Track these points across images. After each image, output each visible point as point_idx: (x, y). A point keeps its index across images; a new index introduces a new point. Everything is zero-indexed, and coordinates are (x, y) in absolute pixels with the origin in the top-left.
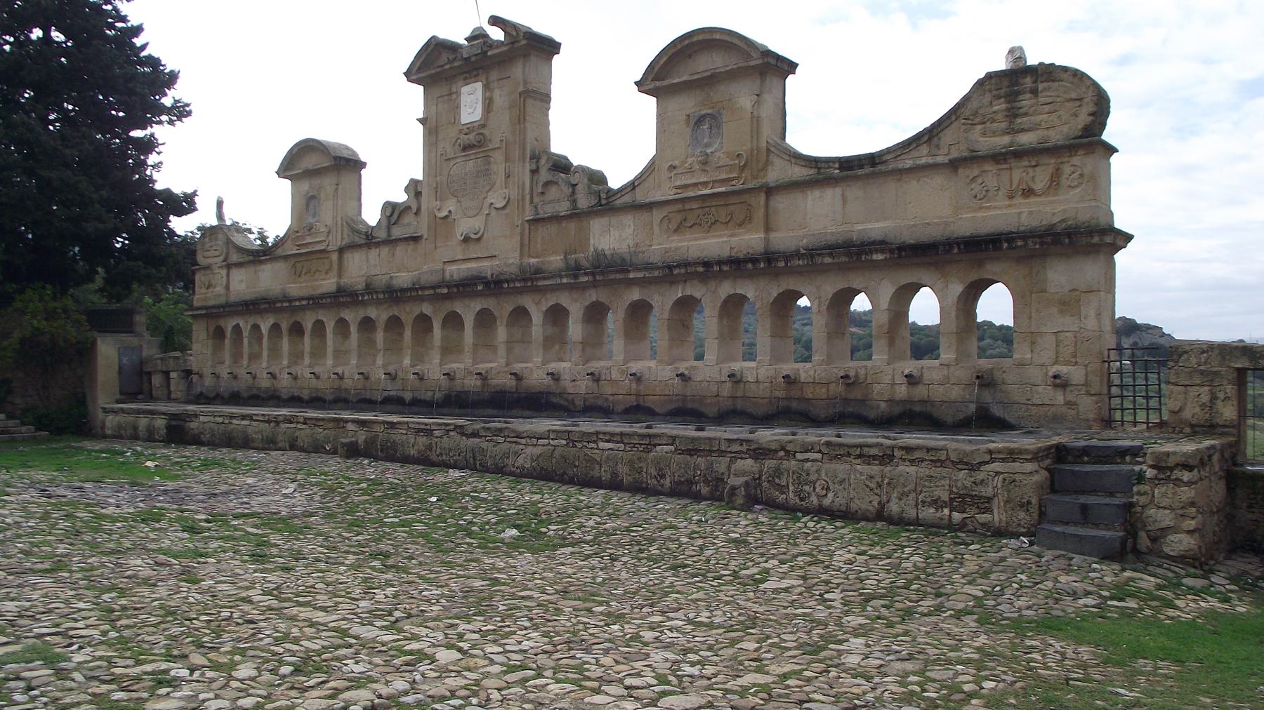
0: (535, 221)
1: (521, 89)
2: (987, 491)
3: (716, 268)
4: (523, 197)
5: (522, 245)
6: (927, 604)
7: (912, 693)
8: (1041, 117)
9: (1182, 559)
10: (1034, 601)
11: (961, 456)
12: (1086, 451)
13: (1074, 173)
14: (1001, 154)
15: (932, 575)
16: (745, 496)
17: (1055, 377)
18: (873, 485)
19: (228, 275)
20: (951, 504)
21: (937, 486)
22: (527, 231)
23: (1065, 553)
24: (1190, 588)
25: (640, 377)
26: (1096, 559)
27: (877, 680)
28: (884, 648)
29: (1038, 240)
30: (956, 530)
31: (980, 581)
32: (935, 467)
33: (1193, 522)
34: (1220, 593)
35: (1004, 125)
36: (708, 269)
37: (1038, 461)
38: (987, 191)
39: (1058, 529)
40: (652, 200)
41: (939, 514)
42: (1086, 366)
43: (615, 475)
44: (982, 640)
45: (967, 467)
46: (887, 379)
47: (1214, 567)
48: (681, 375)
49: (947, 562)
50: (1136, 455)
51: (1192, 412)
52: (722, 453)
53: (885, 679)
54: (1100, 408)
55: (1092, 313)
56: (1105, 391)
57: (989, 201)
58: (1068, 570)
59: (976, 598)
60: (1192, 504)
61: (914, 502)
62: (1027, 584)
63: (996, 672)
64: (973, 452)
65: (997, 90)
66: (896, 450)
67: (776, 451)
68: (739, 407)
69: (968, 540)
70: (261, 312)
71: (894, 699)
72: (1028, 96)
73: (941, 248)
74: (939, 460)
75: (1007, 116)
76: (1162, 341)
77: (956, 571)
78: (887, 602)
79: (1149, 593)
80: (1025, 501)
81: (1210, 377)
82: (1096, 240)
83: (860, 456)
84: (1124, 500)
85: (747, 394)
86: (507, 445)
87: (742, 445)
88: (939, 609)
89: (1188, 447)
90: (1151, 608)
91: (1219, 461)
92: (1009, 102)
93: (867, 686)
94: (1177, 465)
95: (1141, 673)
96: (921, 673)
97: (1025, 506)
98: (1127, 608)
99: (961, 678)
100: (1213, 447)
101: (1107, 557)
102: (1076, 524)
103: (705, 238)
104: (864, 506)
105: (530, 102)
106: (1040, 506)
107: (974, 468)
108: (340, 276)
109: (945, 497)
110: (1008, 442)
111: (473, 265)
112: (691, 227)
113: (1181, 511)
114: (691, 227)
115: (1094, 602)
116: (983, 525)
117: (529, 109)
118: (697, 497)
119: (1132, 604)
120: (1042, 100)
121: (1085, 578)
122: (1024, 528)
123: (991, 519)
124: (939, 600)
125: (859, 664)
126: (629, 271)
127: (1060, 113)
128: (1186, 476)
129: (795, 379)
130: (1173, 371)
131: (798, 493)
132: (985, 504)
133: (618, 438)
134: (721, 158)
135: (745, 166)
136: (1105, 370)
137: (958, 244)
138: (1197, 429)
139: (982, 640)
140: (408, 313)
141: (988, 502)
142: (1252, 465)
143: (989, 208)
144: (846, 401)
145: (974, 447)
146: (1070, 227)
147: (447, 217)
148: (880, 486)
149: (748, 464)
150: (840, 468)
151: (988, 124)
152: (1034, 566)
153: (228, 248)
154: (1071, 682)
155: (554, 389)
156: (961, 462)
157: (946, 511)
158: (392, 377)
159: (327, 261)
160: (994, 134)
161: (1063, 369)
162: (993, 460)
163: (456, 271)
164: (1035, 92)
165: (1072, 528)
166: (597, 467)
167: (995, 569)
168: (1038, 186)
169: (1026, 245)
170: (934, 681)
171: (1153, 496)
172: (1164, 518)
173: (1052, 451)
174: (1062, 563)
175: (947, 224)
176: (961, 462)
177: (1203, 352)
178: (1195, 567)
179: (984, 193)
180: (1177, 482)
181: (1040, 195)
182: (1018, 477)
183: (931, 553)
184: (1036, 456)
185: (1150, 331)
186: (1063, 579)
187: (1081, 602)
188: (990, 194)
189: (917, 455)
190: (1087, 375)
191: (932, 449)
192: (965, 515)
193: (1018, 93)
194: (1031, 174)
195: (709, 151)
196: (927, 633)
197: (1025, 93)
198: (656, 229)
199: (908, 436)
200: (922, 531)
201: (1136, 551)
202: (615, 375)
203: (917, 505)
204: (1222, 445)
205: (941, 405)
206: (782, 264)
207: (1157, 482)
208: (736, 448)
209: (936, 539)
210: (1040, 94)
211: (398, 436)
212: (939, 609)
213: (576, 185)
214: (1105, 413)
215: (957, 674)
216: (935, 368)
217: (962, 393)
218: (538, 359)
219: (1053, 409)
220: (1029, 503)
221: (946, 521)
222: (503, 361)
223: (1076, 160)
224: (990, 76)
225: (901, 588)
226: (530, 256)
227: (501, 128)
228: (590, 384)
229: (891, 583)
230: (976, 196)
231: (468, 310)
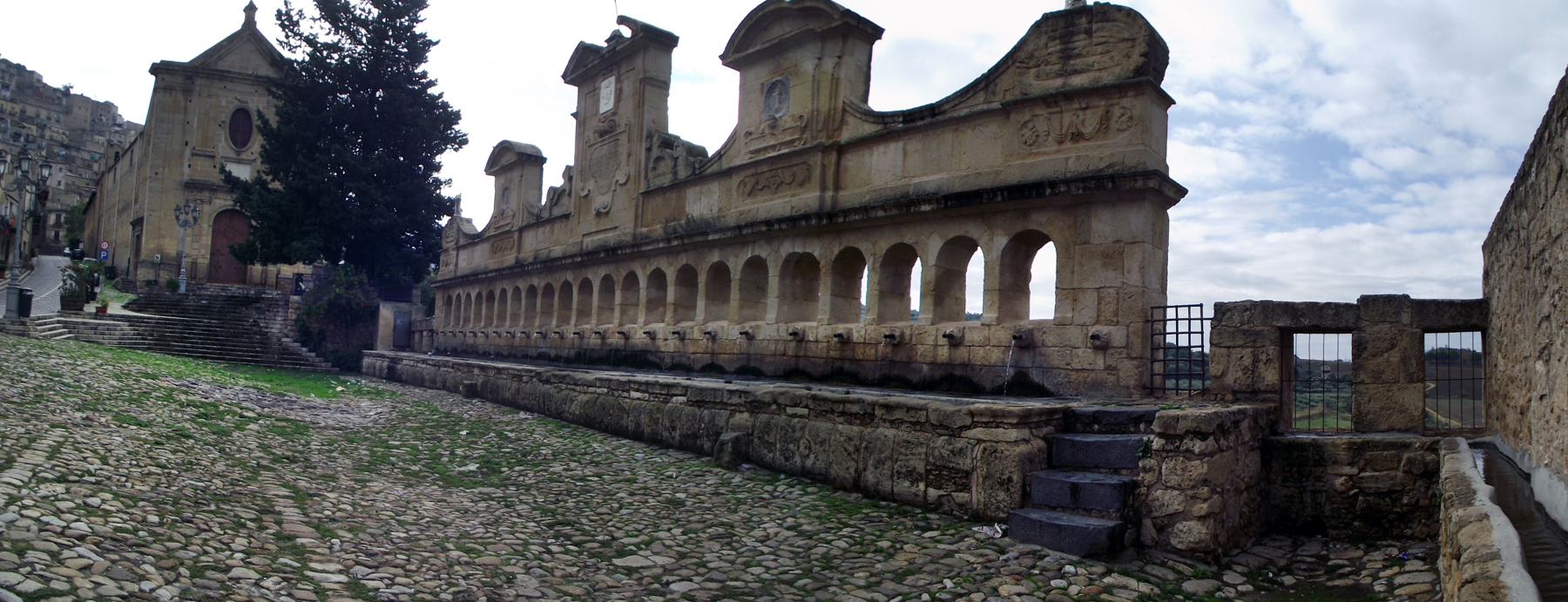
0: (648, 194)
1: (641, 76)
2: (965, 463)
3: (776, 227)
4: (639, 173)
5: (636, 217)
8: (1093, 58)
12: (1096, 417)
13: (1123, 115)
14: (1052, 95)
16: (732, 453)
17: (1093, 337)
18: (851, 449)
19: (457, 255)
21: (913, 454)
22: (641, 204)
25: (715, 336)
26: (1075, 558)
29: (1081, 185)
32: (915, 431)
33: (1205, 506)
35: (1057, 67)
36: (771, 229)
37: (1030, 428)
38: (1037, 136)
40: (732, 165)
41: (913, 489)
42: (1128, 326)
43: (638, 425)
45: (947, 432)
46: (930, 340)
48: (746, 333)
52: (724, 405)
54: (1141, 373)
55: (1135, 267)
57: (1039, 147)
64: (953, 413)
65: (1053, 31)
66: (876, 407)
67: (769, 404)
68: (801, 366)
70: (471, 283)
72: (1083, 36)
73: (986, 196)
74: (918, 423)
75: (1061, 58)
80: (1005, 477)
82: (1139, 184)
83: (843, 414)
85: (809, 354)
86: (567, 392)
87: (740, 397)
91: (1251, 429)
92: (1064, 43)
94: (1187, 432)
97: (1006, 484)
102: (1064, 509)
103: (772, 200)
104: (842, 473)
105: (648, 88)
106: (1024, 486)
107: (955, 433)
108: (519, 251)
109: (921, 468)
111: (601, 236)
112: (762, 190)
113: (1190, 490)
114: (762, 190)
116: (961, 505)
117: (647, 95)
118: (699, 452)
120: (1095, 40)
122: (1004, 512)
123: (969, 499)
126: (708, 235)
127: (1113, 54)
128: (1198, 446)
129: (849, 338)
131: (784, 451)
132: (962, 480)
133: (643, 388)
134: (787, 122)
135: (806, 126)
138: (1239, 396)
140: (557, 280)
143: (1037, 154)
144: (893, 363)
145: (958, 408)
147: (587, 196)
148: (857, 450)
149: (743, 418)
150: (823, 425)
151: (1042, 67)
153: (458, 234)
155: (650, 348)
156: (941, 426)
157: (922, 486)
158: (544, 336)
159: (511, 240)
160: (1048, 76)
161: (1103, 329)
162: (974, 425)
163: (590, 242)
164: (1089, 33)
166: (626, 416)
168: (1088, 130)
169: (1068, 191)
171: (1160, 473)
173: (1056, 417)
175: (997, 173)
176: (941, 426)
177: (1247, 310)
178: (1208, 564)
179: (1034, 138)
180: (1188, 455)
181: (1089, 140)
182: (1001, 447)
188: (1040, 140)
189: (898, 415)
190: (1128, 336)
192: (942, 492)
193: (1073, 34)
194: (1081, 117)
195: (777, 116)
197: (1079, 33)
198: (734, 193)
202: (697, 335)
203: (892, 476)
206: (841, 220)
207: (1164, 455)
208: (735, 400)
210: (1094, 35)
211: (504, 381)
213: (677, 158)
214: (1146, 379)
216: (977, 328)
217: (1002, 356)
218: (641, 320)
219: (1093, 375)
221: (920, 499)
222: (616, 321)
223: (1126, 102)
224: (1047, 17)
226: (642, 226)
227: (626, 115)
228: (677, 342)
230: (1026, 142)
231: (596, 276)
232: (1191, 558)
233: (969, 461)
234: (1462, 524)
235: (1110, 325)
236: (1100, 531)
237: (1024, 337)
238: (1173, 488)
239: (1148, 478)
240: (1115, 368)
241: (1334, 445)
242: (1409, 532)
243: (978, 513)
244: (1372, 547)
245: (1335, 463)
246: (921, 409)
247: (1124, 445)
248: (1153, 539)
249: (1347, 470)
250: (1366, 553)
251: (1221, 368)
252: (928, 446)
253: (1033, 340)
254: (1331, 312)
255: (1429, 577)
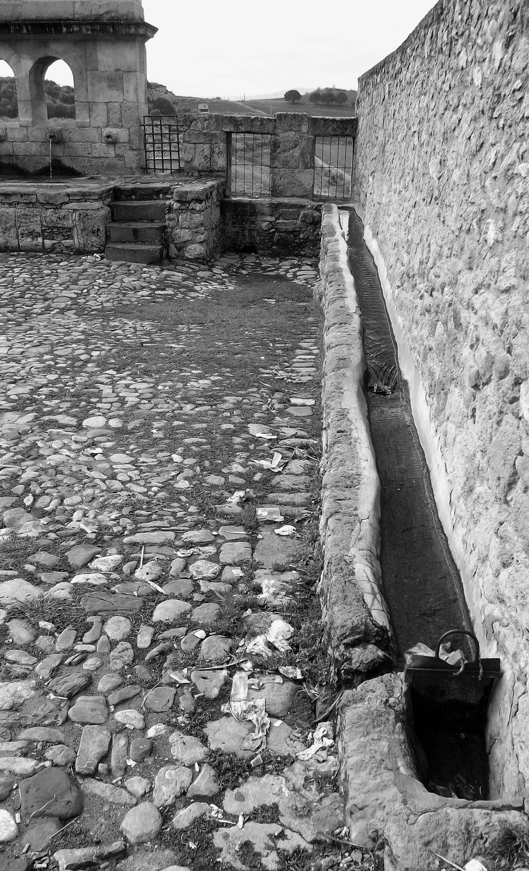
2: (68, 223)
6: (39, 307)
7: (50, 366)
9: (196, 260)
10: (110, 296)
11: (47, 199)
12: (133, 191)
15: (38, 286)
17: (108, 137)
20: (43, 234)
23: (124, 262)
24: (202, 278)
26: (145, 265)
27: (23, 361)
28: (20, 341)
29: (89, 27)
30: (48, 253)
31: (72, 287)
32: (29, 207)
33: (202, 236)
34: (219, 279)
39: (119, 246)
41: (35, 242)
44: (83, 326)
47: (215, 263)
49: (47, 276)
50: (166, 193)
51: (199, 162)
53: (29, 360)
55: (132, 89)
56: (143, 147)
58: (129, 274)
59: (71, 298)
60: (202, 225)
61: (15, 235)
62: (104, 286)
63: (98, 345)
64: (56, 195)
69: (58, 259)
71: (39, 372)
74: (31, 203)
76: (166, 96)
77: (54, 281)
78: (11, 309)
79: (179, 283)
81: (210, 138)
82: (132, 31)
84: (160, 224)
88: (48, 309)
89: (198, 187)
90: (182, 293)
91: (217, 195)
93: (19, 367)
94: (193, 200)
95: (182, 333)
96: (51, 352)
97: (97, 232)
98: (167, 295)
99: (77, 352)
100: (213, 186)
101: (152, 263)
102: (130, 242)
107: (57, 207)
109: (38, 229)
110: (79, 187)
113: (195, 229)
115: (147, 293)
116: (67, 247)
119: (170, 291)
121: (140, 278)
124: (47, 303)
125: (7, 353)
128: (198, 207)
130: (186, 133)
132: (67, 232)
136: (142, 132)
137: (27, 26)
138: (202, 173)
139: (83, 326)
141: (70, 231)
142: (235, 196)
145: (57, 192)
146: (113, 18)
152: (106, 273)
154: (144, 345)
156: (48, 203)
157: (40, 240)
161: (113, 131)
162: (70, 201)
165: (128, 245)
167: (80, 277)
169: (81, 30)
170: (61, 356)
171: (178, 221)
172: (184, 234)
174: (124, 269)
176: (48, 203)
177: (206, 120)
178: (204, 265)
180: (193, 211)
182: (90, 213)
183: (34, 270)
184: (101, 197)
185: (158, 89)
186: (126, 280)
187: (140, 294)
189: (13, 199)
190: (129, 135)
191: (25, 194)
192: (55, 242)
196: (46, 326)
199: (3, 184)
200: (23, 255)
201: (169, 258)
203: (17, 237)
204: (218, 185)
205: (24, 159)
207: (180, 211)
209: (35, 260)
212: (48, 309)
215: (74, 350)
219: (107, 161)
220: (98, 230)
221: (41, 247)
225: (18, 297)
229: (10, 295)
232: (196, 262)
233: (70, 222)
234: (329, 242)
235: (117, 127)
236: (156, 251)
237: (56, 135)
238: (186, 228)
239: (172, 223)
240: (122, 156)
241: (262, 204)
242: (303, 253)
243: (80, 250)
244: (282, 259)
245: (262, 214)
246: (32, 195)
247: (156, 206)
248: (176, 254)
249: (269, 218)
250: (280, 262)
251: (190, 156)
252: (41, 216)
253: (62, 138)
254: (258, 123)
255: (315, 273)
